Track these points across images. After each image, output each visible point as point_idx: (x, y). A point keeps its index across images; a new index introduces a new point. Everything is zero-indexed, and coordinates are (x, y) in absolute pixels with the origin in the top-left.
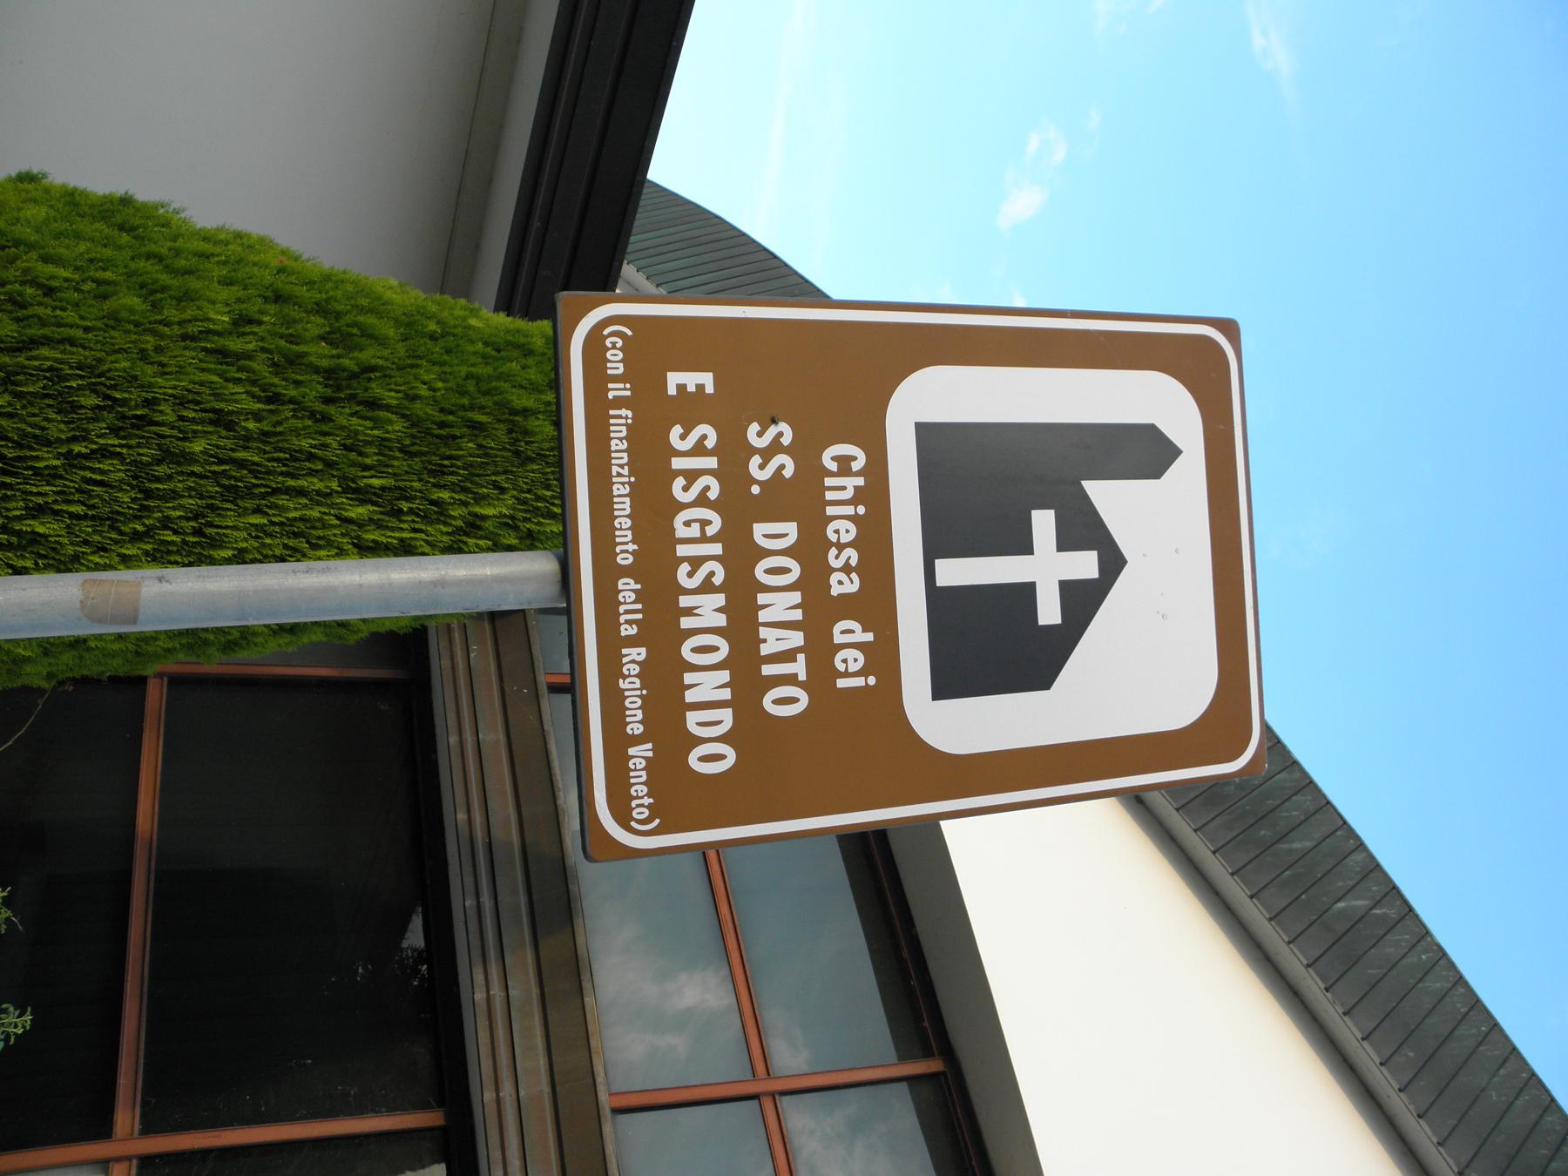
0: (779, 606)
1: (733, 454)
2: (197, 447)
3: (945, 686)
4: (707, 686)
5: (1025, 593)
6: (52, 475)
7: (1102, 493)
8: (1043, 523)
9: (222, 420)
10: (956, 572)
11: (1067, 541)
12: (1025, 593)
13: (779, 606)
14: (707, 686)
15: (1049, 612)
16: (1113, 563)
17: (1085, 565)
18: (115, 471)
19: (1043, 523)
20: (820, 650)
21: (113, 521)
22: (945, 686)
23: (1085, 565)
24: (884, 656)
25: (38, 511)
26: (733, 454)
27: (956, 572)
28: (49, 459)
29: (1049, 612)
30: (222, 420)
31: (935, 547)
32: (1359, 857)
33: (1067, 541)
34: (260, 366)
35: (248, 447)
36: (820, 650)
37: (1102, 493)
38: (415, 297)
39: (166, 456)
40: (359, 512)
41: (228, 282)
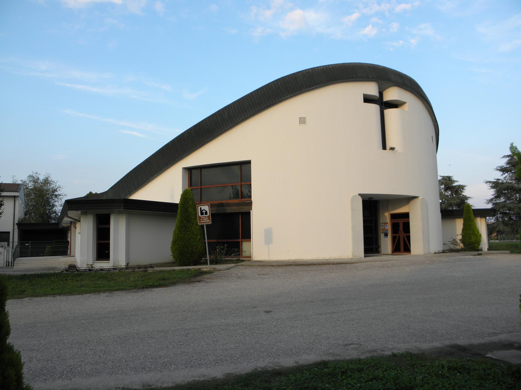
0: (205, 219)
1: (202, 220)
2: (191, 235)
3: (207, 214)
4: (207, 221)
5: (205, 212)
6: (193, 243)
7: (202, 210)
8: (203, 212)
9: (189, 234)
10: (204, 214)
11: (203, 211)
12: (205, 212)
13: (205, 219)
14: (207, 221)
15: (205, 211)
16: (204, 209)
17: (204, 210)
18: (192, 240)
19: (203, 212)
20: (207, 218)
21: (195, 240)
22: (207, 214)
23: (204, 210)
24: (207, 216)
25: (195, 244)
26: (202, 220)
27: (204, 214)
28: (192, 243)
29: (205, 211)
30: (189, 234)
31: (204, 215)
32: (170, 144)
33: (203, 211)
34: (185, 232)
35: (239, 260)
36: (207, 218)
37: (202, 210)
38: (177, 221)
39: (191, 237)
40: (194, 226)
41: (179, 235)
